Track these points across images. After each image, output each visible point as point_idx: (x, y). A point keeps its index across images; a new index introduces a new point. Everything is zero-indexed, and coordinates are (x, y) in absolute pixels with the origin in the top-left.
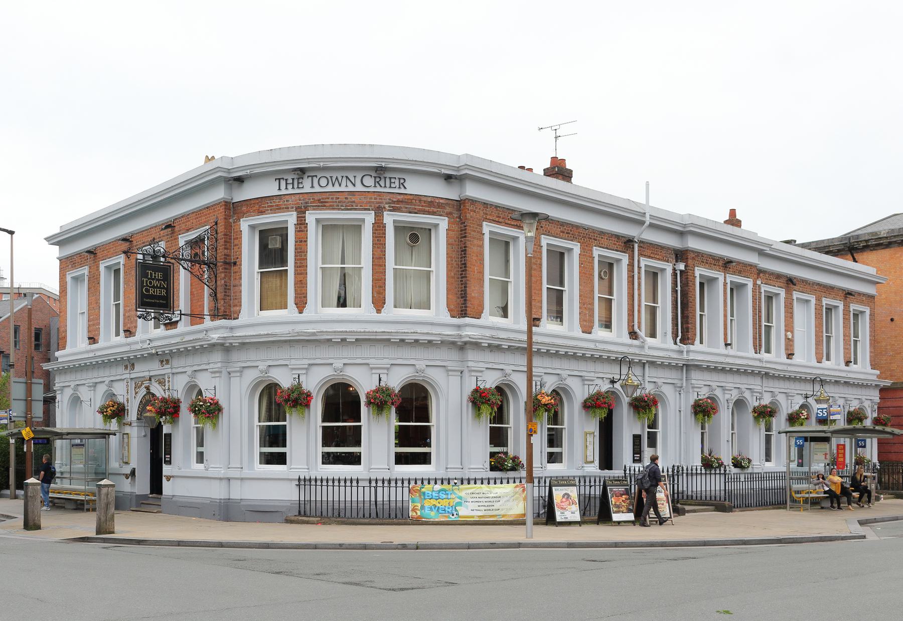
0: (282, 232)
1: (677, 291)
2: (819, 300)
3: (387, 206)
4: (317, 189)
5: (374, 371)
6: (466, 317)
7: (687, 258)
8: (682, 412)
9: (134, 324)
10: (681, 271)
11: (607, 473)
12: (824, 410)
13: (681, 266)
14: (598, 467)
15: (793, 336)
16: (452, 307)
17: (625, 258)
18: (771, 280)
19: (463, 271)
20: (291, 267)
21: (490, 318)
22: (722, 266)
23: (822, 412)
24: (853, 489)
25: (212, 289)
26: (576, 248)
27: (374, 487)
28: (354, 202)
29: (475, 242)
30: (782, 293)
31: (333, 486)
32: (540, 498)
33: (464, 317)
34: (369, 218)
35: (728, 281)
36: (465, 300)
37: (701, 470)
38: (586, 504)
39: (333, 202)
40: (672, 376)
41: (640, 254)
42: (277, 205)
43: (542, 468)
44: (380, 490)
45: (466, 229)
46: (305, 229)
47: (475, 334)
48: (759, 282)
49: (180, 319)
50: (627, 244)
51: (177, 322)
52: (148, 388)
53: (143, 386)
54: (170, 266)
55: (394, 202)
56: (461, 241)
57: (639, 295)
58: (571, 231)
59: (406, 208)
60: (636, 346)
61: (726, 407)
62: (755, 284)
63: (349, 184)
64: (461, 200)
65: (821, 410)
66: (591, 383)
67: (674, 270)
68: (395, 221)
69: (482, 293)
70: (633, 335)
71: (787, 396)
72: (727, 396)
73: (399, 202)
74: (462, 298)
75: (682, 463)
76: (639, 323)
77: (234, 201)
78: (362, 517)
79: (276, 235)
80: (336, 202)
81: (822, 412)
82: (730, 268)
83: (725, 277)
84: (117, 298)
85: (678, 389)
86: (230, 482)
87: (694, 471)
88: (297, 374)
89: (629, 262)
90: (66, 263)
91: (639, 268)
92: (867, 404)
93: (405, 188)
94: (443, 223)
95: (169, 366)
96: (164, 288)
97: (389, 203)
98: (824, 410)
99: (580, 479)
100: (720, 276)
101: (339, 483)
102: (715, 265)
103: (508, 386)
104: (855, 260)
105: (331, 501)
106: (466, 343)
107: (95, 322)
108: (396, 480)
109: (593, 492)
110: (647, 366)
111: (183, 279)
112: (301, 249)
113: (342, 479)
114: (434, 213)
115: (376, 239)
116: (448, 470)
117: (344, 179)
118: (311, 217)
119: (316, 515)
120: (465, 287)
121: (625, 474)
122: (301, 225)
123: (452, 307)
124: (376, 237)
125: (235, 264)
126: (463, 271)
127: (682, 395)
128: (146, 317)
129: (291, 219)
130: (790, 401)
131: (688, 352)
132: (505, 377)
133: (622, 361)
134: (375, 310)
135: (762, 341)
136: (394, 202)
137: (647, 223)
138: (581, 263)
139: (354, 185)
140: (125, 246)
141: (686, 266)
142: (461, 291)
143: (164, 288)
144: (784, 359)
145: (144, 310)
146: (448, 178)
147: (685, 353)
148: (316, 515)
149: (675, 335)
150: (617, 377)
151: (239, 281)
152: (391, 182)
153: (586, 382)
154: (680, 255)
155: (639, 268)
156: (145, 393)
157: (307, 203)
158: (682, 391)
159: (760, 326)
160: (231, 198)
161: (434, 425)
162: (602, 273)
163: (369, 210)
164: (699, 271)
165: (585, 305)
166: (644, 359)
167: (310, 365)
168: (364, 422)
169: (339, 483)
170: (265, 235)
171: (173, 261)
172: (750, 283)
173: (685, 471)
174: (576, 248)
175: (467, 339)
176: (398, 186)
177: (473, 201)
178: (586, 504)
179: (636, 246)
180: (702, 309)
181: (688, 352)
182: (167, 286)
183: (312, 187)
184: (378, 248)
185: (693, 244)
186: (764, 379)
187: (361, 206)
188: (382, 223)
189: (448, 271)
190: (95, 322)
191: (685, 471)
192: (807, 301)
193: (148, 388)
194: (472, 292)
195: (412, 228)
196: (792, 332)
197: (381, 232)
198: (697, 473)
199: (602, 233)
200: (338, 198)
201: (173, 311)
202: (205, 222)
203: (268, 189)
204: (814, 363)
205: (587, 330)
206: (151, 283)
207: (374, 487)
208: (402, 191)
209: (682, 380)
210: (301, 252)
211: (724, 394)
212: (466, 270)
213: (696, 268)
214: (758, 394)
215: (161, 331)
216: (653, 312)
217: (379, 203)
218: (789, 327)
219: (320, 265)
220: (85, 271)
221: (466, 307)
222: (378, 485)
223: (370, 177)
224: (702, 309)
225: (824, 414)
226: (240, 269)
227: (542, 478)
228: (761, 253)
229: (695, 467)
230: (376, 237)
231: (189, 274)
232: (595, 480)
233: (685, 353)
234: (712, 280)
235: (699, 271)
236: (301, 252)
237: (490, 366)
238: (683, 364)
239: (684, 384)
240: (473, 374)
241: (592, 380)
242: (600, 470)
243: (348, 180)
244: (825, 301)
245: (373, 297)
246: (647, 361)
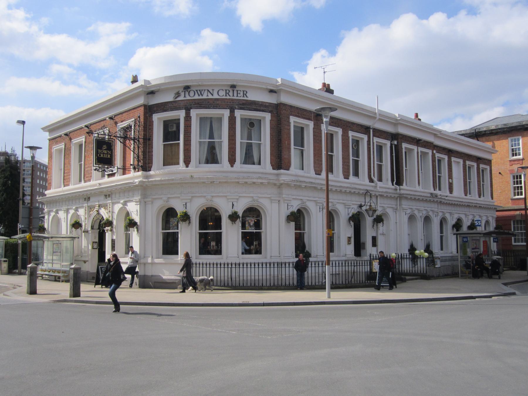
0: (177, 122)
1: (393, 156)
2: (464, 162)
3: (237, 107)
4: (188, 98)
5: (229, 200)
6: (281, 169)
7: (398, 138)
8: (398, 223)
9: (90, 175)
10: (395, 145)
11: (358, 259)
12: (479, 222)
13: (396, 142)
14: (354, 255)
15: (452, 182)
16: (273, 163)
17: (365, 137)
18: (440, 151)
19: (279, 143)
20: (181, 142)
21: (294, 170)
22: (416, 143)
23: (478, 223)
24: (478, 266)
25: (136, 154)
26: (340, 131)
27: (230, 268)
28: (218, 104)
29: (286, 127)
30: (446, 157)
31: (224, 267)
32: (323, 273)
33: (280, 169)
34: (226, 113)
35: (419, 151)
36: (281, 160)
37: (409, 256)
38: (352, 276)
39: (206, 104)
40: (393, 203)
41: (374, 136)
42: (174, 106)
43: (323, 256)
44: (233, 269)
45: (281, 120)
46: (190, 120)
47: (287, 179)
48: (435, 152)
49: (117, 172)
50: (366, 130)
51: (115, 173)
52: (98, 211)
53: (95, 210)
54: (113, 141)
55: (240, 104)
56: (278, 127)
57: (374, 158)
58: (337, 122)
59: (247, 108)
60: (372, 186)
61: (420, 220)
62: (433, 153)
63: (209, 94)
64: (278, 104)
65: (477, 222)
66: (349, 207)
67: (391, 145)
68: (241, 115)
69: (290, 156)
70: (371, 181)
71: (451, 214)
72: (421, 214)
73: (243, 104)
74: (279, 158)
75: (398, 252)
76: (374, 173)
77: (149, 104)
78: (223, 286)
79: (173, 123)
80: (208, 104)
81: (478, 223)
82: (420, 144)
83: (418, 149)
84: (80, 160)
85: (395, 211)
86: (145, 267)
87: (405, 257)
88: (184, 202)
89: (368, 140)
90: (53, 141)
91: (373, 143)
92: (490, 219)
93: (247, 97)
94: (268, 117)
95: (110, 198)
96: (109, 154)
97: (238, 105)
98: (479, 222)
99: (342, 262)
100: (415, 148)
101: (196, 265)
102: (412, 142)
103: (304, 208)
104: (478, 140)
105: (288, 275)
106: (281, 184)
107: (68, 174)
108: (274, 263)
109: (350, 269)
110: (379, 198)
111: (118, 147)
112: (188, 130)
113: (230, 263)
114: (263, 111)
115: (231, 125)
116: (272, 257)
117: (206, 91)
118: (194, 113)
119: (217, 285)
120: (281, 152)
121: (370, 258)
122: (188, 118)
123: (273, 163)
124: (231, 124)
125: (149, 139)
126: (279, 143)
127: (397, 214)
128: (99, 170)
129: (181, 114)
130: (467, 218)
131: (400, 189)
132: (303, 203)
133: (367, 193)
134: (230, 165)
135: (437, 183)
136: (240, 104)
137: (378, 118)
138: (343, 140)
139: (212, 95)
140: (87, 130)
141: (397, 142)
142: (278, 155)
143: (109, 154)
144: (448, 193)
145: (98, 166)
146: (271, 91)
147: (398, 190)
148: (217, 285)
149: (392, 181)
150: (363, 204)
151: (152, 150)
152: (237, 93)
153: (347, 207)
154: (394, 137)
155: (373, 143)
156: (96, 214)
157: (191, 105)
158: (397, 211)
159: (436, 176)
160: (147, 103)
161: (263, 232)
162: (354, 145)
163: (226, 108)
164: (404, 145)
165: (345, 164)
166: (377, 194)
167: (192, 197)
168: (224, 230)
169: (196, 265)
170: (167, 124)
171: (114, 138)
172: (430, 152)
173: (400, 257)
174: (340, 131)
175: (282, 182)
176: (242, 96)
177: (284, 105)
178: (352, 276)
179: (371, 131)
180: (406, 167)
181: (400, 189)
182: (111, 152)
183: (185, 97)
184: (232, 130)
185: (402, 131)
186: (439, 204)
187: (222, 107)
188: (234, 116)
189: (271, 143)
190: (68, 174)
191: (400, 257)
192: (458, 163)
193: (98, 211)
194: (285, 155)
195: (250, 119)
196: (452, 179)
197: (233, 121)
198: (373, 258)
199: (353, 124)
200: (209, 102)
201: (114, 167)
202: (133, 116)
203: (169, 98)
204: (463, 195)
205: (346, 177)
206: (102, 152)
207: (230, 268)
208: (245, 98)
209: (397, 205)
210: (187, 133)
211: (419, 213)
212: (281, 143)
213: (403, 144)
214: (436, 213)
215: (106, 179)
216: (380, 167)
217: (232, 105)
218: (450, 176)
219: (198, 140)
220: (62, 146)
221: (281, 163)
222: (233, 266)
223: (222, 91)
224: (406, 167)
225: (479, 224)
226: (152, 142)
227: (324, 261)
228: (435, 135)
229: (406, 254)
230: (231, 124)
231: (122, 145)
232: (351, 263)
233: (398, 190)
234: (411, 150)
235: (404, 145)
236: (187, 133)
237: (294, 197)
238: (398, 197)
239: (398, 208)
240: (286, 202)
241: (350, 205)
242: (355, 257)
243: (209, 93)
244: (468, 163)
245: (229, 158)
246: (379, 195)
